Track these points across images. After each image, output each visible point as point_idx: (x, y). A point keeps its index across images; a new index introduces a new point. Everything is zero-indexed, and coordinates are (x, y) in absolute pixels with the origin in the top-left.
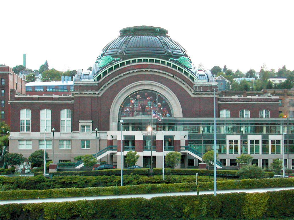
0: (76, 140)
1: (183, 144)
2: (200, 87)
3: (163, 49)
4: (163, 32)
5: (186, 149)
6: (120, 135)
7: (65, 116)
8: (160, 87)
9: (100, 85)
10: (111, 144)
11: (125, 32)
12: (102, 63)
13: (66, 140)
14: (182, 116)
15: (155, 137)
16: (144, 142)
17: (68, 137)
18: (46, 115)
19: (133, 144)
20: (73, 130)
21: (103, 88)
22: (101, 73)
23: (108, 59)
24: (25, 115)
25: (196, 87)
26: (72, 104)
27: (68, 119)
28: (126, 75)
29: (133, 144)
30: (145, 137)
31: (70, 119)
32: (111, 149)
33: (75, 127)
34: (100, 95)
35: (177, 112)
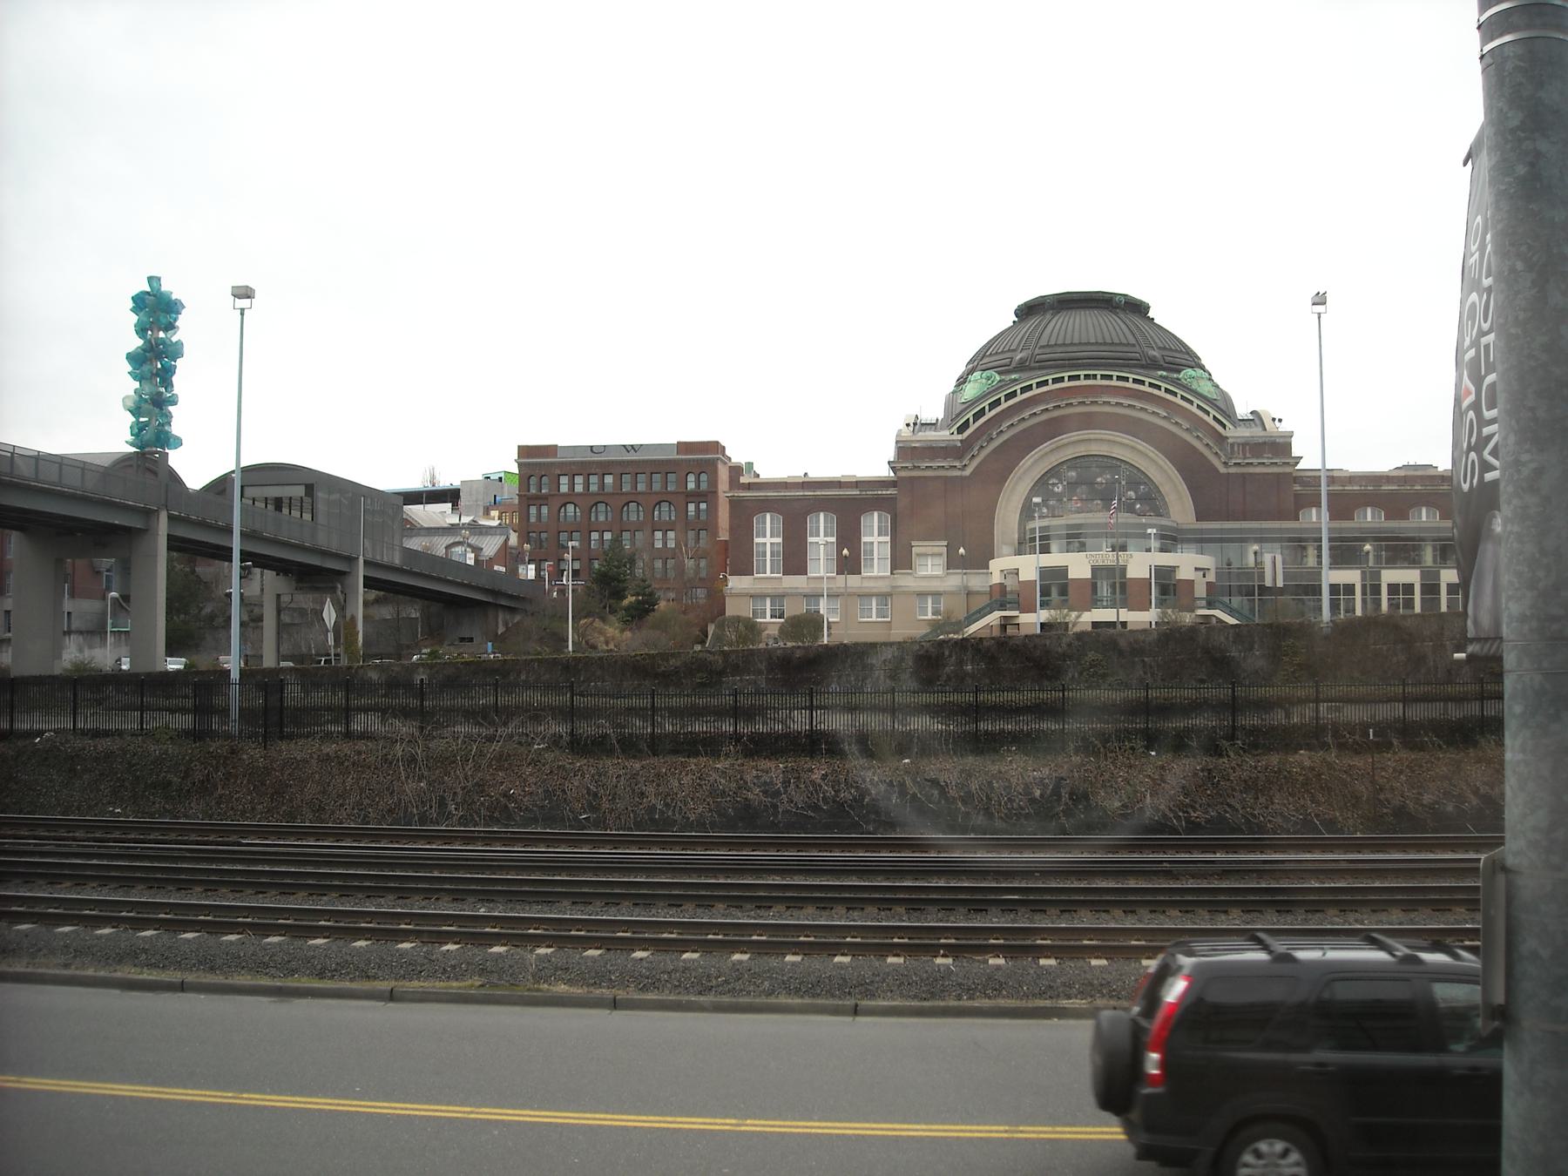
0: (904, 593)
1: (1200, 591)
2: (1244, 445)
3: (1137, 349)
4: (1137, 308)
5: (1210, 605)
6: (1029, 567)
7: (875, 535)
8: (1133, 448)
9: (967, 445)
10: (1001, 597)
11: (1028, 311)
12: (970, 391)
13: (877, 595)
14: (1191, 517)
15: (1124, 570)
16: (1093, 585)
17: (883, 587)
18: (821, 539)
19: (1063, 591)
20: (894, 567)
21: (975, 452)
22: (970, 415)
23: (988, 378)
24: (768, 538)
25: (1232, 445)
26: (892, 499)
27: (882, 539)
28: (1037, 416)
29: (1063, 591)
30: (1095, 569)
31: (888, 539)
32: (1002, 607)
33: (901, 560)
34: (967, 472)
35: (1181, 510)
